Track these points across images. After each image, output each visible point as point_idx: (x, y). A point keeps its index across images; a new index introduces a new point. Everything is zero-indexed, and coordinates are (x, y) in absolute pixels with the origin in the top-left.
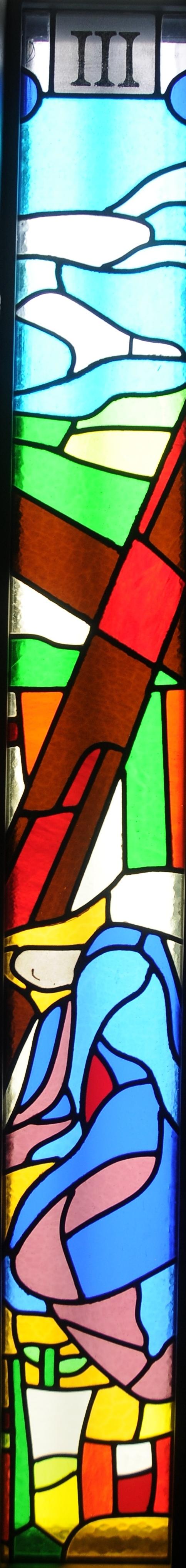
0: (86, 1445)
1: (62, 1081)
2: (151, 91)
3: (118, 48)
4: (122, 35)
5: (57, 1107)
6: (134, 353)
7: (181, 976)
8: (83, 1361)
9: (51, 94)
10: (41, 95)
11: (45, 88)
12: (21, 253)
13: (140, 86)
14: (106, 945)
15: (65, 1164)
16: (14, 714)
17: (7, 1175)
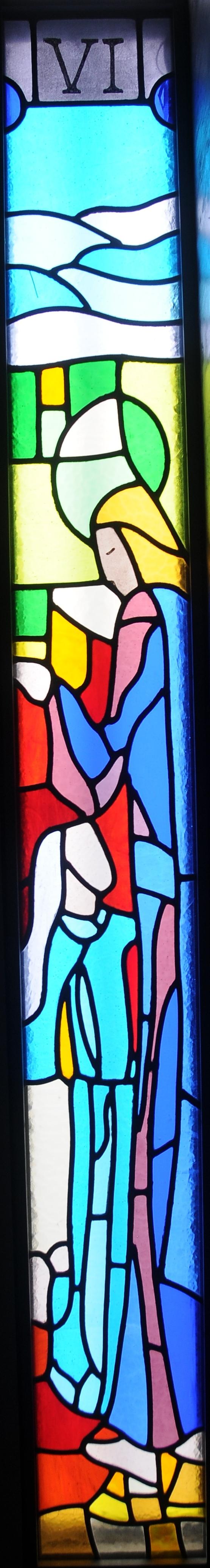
0: (112, 364)
2: (135, 96)
3: (101, 50)
4: (105, 42)
6: (119, 447)
7: (187, 543)
8: (65, 919)
9: (36, 103)
10: (25, 105)
11: (29, 98)
12: (21, 634)
14: (114, 487)
17: (13, 465)
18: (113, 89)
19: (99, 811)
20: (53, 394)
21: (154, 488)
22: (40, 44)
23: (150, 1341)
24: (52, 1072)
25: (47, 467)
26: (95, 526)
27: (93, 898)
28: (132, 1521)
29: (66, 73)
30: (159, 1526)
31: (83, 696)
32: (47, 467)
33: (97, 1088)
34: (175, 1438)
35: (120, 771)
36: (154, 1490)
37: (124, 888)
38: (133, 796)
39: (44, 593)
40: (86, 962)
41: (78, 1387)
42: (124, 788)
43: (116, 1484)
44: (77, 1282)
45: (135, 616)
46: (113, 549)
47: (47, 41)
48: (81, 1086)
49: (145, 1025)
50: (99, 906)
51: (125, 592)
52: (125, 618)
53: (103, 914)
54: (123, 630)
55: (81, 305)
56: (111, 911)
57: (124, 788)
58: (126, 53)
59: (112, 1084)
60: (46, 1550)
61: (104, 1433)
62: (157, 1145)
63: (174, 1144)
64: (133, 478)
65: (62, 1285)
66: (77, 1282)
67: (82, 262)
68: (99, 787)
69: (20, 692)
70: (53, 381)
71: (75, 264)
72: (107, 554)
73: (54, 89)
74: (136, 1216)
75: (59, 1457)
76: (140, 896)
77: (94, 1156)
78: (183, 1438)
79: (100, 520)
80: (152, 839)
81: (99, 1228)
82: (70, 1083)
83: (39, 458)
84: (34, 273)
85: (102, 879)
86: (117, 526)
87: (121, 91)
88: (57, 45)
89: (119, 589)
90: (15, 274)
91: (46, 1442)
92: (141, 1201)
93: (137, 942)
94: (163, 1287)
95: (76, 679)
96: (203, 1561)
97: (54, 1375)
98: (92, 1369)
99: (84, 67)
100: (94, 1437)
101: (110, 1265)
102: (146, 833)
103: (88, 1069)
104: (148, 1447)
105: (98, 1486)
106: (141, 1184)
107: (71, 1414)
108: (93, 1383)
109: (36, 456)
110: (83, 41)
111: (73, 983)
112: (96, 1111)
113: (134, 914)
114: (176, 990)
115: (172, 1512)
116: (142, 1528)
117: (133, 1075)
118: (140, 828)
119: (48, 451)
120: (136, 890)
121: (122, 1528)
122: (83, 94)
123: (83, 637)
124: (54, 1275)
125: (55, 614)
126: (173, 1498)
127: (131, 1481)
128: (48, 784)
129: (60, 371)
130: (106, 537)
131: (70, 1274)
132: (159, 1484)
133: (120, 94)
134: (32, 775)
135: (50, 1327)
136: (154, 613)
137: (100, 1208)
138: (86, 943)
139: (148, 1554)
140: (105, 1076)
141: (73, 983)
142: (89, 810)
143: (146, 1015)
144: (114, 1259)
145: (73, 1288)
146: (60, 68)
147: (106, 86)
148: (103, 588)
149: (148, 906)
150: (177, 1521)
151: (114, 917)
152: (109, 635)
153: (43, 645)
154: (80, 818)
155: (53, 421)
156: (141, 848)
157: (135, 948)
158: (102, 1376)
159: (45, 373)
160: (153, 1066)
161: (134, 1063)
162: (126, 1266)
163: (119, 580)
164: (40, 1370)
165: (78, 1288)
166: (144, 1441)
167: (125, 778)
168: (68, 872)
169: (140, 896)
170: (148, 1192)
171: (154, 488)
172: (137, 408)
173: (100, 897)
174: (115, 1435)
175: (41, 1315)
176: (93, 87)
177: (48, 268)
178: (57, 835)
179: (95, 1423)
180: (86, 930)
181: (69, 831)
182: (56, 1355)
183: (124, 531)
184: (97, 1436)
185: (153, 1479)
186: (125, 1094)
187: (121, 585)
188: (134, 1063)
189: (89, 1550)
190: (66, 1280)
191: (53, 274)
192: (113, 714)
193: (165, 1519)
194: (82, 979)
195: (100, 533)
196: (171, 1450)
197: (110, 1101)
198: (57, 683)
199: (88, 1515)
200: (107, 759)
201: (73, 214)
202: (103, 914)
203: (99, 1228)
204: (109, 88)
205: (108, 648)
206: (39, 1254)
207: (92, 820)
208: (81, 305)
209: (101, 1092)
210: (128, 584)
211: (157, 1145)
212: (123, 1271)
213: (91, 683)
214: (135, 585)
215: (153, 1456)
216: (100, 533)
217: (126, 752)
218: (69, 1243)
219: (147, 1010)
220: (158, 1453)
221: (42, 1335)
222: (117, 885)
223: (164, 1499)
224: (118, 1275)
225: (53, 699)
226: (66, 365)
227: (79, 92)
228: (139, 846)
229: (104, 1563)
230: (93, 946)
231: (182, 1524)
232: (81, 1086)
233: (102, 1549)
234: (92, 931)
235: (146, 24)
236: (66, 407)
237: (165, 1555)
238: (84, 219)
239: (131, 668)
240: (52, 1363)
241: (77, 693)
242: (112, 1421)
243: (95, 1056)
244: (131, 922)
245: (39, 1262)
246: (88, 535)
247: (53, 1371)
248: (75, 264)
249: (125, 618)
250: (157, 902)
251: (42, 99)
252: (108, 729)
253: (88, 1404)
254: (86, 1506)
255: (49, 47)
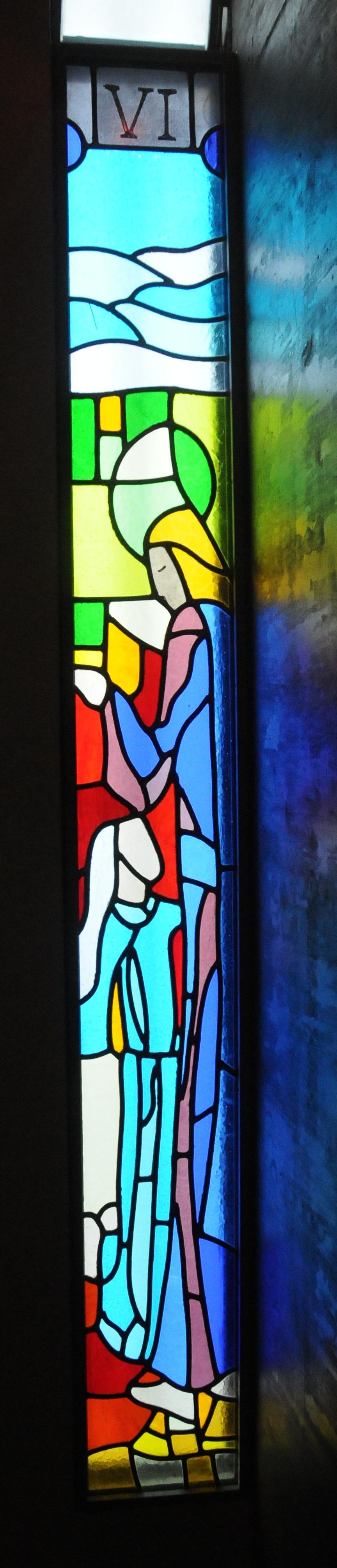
1: (134, 779)
2: (186, 144)
3: (156, 99)
4: (160, 91)
5: (191, 681)
6: (170, 473)
8: (118, 906)
9: (96, 145)
10: (85, 147)
11: (89, 140)
13: (177, 141)
15: (109, 767)
16: (93, 776)
18: (166, 136)
19: (150, 807)
20: (111, 420)
21: (202, 512)
22: (100, 88)
23: (190, 1291)
24: (104, 1046)
25: (105, 489)
26: (148, 545)
27: (142, 886)
28: (172, 1455)
29: (124, 119)
30: (196, 1459)
31: (135, 701)
32: (105, 489)
33: (144, 1061)
34: (211, 1378)
35: (168, 771)
36: (191, 1427)
37: (170, 877)
38: (180, 794)
39: (100, 606)
40: (136, 946)
41: (124, 1335)
42: (172, 786)
43: (158, 1424)
44: (125, 1239)
45: (183, 629)
46: (164, 567)
47: (107, 87)
48: (130, 1059)
49: (189, 1003)
50: (149, 894)
51: (175, 607)
52: (174, 630)
53: (152, 901)
54: (173, 642)
55: (136, 339)
56: (159, 899)
57: (172, 786)
58: (179, 103)
59: (158, 1057)
60: (95, 1486)
61: (148, 1377)
62: (198, 1112)
63: (213, 1110)
64: (182, 502)
65: (111, 1242)
66: (125, 1239)
67: (138, 298)
68: (149, 786)
69: (78, 698)
70: (110, 409)
71: (131, 300)
72: (159, 571)
73: (113, 133)
74: (178, 1177)
75: (105, 1401)
76: (186, 885)
77: (142, 1123)
78: (218, 1379)
79: (152, 540)
80: (197, 833)
81: (145, 1188)
82: (120, 1057)
83: (97, 480)
84: (93, 306)
85: (151, 869)
86: (168, 546)
87: (174, 139)
88: (116, 92)
89: (170, 603)
90: (73, 305)
91: (92, 1386)
92: (183, 1163)
93: (182, 927)
94: (201, 1241)
95: (130, 686)
96: (236, 1487)
97: (103, 1326)
98: (137, 1319)
99: (141, 114)
100: (138, 1381)
101: (155, 1222)
102: (191, 827)
103: (136, 1043)
104: (187, 1388)
105: (142, 1424)
106: (183, 1148)
107: (118, 1361)
108: (138, 1331)
109: (94, 479)
110: (140, 89)
111: (124, 965)
112: (143, 1081)
113: (180, 901)
114: (216, 971)
115: (207, 1446)
116: (180, 1461)
117: (177, 1048)
118: (186, 823)
119: (106, 475)
120: (182, 879)
121: (163, 1463)
122: (139, 139)
123: (136, 647)
124: (104, 1233)
125: (111, 626)
126: (208, 1434)
127: (171, 1419)
128: (103, 782)
129: (117, 400)
130: (158, 556)
131: (118, 1232)
132: (196, 1421)
133: (173, 142)
134: (87, 773)
135: (100, 1281)
136: (200, 627)
137: (146, 1170)
138: (136, 928)
139: (186, 1485)
140: (152, 1050)
141: (124, 965)
142: (140, 806)
143: (189, 994)
144: (159, 1217)
145: (121, 1245)
146: (118, 113)
147: (161, 133)
148: (155, 603)
149: (192, 895)
150: (212, 1453)
151: (162, 905)
152: (160, 646)
153: (99, 654)
154: (132, 813)
155: (111, 446)
156: (187, 842)
157: (180, 933)
158: (146, 1325)
159: (103, 400)
160: (195, 1040)
161: (178, 1038)
162: (169, 1224)
163: (169, 596)
164: (90, 1323)
165: (125, 1245)
166: (182, 1382)
167: (173, 777)
168: (121, 863)
169: (186, 885)
170: (190, 1155)
171: (202, 512)
172: (187, 437)
173: (150, 885)
174: (158, 1378)
175: (90, 1270)
176: (148, 134)
177: (107, 301)
178: (110, 829)
179: (140, 1368)
180: (136, 916)
181: (122, 826)
182: (105, 1307)
183: (175, 550)
184: (142, 1380)
185: (191, 1416)
186: (170, 1066)
187: (171, 600)
188: (178, 1038)
189: (132, 1485)
190: (115, 1238)
191: (111, 308)
192: (163, 719)
193: (201, 1452)
194: (132, 962)
195: (152, 551)
196: (207, 1390)
197: (157, 1073)
198: (112, 689)
199: (133, 1452)
200: (157, 759)
201: (130, 252)
202: (152, 901)
203: (145, 1188)
204: (163, 135)
205: (159, 658)
206: (90, 1215)
207: (143, 816)
208: (136, 339)
209: (148, 1065)
210: (177, 599)
211: (198, 1112)
212: (166, 1228)
213: (143, 691)
214: (183, 600)
215: (190, 1396)
216: (152, 551)
217: (174, 754)
218: (118, 1204)
219: (190, 989)
220: (196, 1392)
221: (91, 1289)
222: (165, 875)
223: (200, 1434)
224: (162, 1232)
225: (109, 704)
226: (122, 395)
227: (136, 137)
228: (185, 839)
229: (147, 1495)
230: (143, 930)
231: (217, 1456)
232: (130, 1059)
233: (143, 1484)
234: (143, 917)
235: (197, 77)
236: (122, 433)
237: (200, 1484)
238: (140, 258)
239: (179, 676)
240: (102, 1315)
241: (130, 699)
242: (155, 1365)
243: (143, 1031)
244: (177, 909)
245: (89, 1224)
246: (141, 553)
247: (102, 1321)
248: (131, 300)
249: (174, 630)
250: (201, 890)
251: (101, 141)
252: (159, 732)
253: (133, 1351)
254: (130, 1445)
255: (108, 93)
